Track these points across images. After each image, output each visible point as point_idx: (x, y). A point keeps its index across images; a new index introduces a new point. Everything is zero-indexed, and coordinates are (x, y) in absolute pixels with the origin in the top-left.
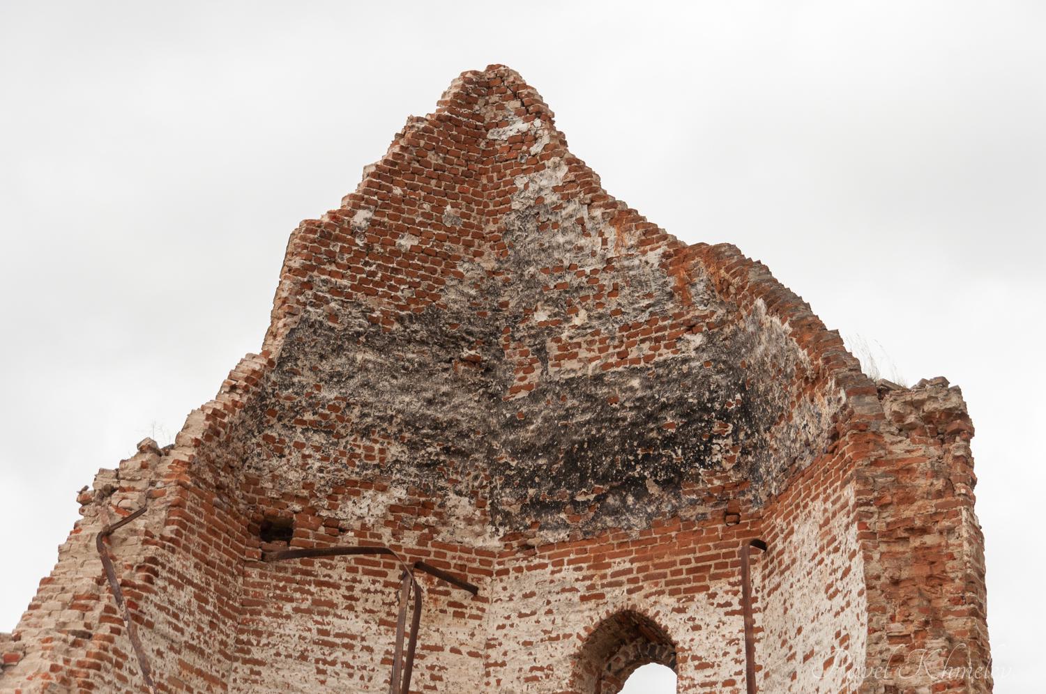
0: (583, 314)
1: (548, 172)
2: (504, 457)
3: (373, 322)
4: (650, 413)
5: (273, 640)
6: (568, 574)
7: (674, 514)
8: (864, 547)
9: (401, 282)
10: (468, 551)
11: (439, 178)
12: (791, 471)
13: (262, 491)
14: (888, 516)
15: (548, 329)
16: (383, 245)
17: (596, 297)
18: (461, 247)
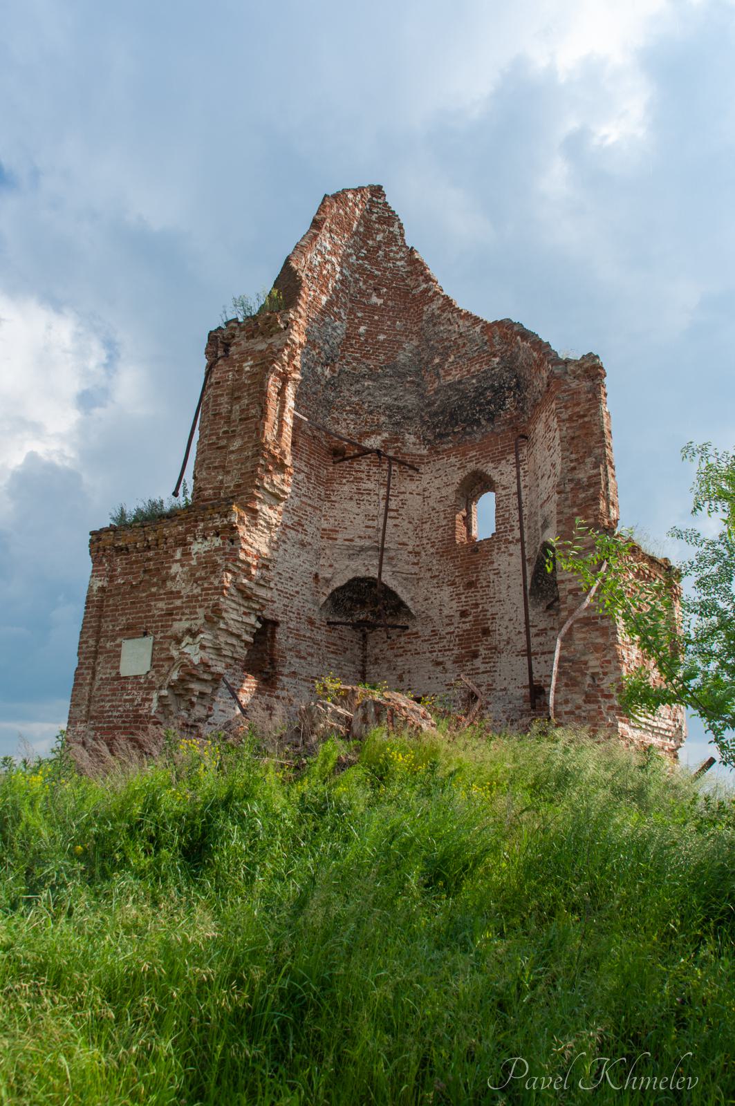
0: (452, 357)
1: (435, 302)
2: (427, 418)
3: (371, 370)
4: (480, 392)
5: (339, 493)
6: (453, 459)
7: (492, 431)
8: (559, 426)
9: (380, 353)
10: (415, 455)
11: (393, 311)
12: (536, 405)
14: (569, 412)
15: (440, 365)
16: (372, 339)
17: (457, 349)
18: (404, 338)
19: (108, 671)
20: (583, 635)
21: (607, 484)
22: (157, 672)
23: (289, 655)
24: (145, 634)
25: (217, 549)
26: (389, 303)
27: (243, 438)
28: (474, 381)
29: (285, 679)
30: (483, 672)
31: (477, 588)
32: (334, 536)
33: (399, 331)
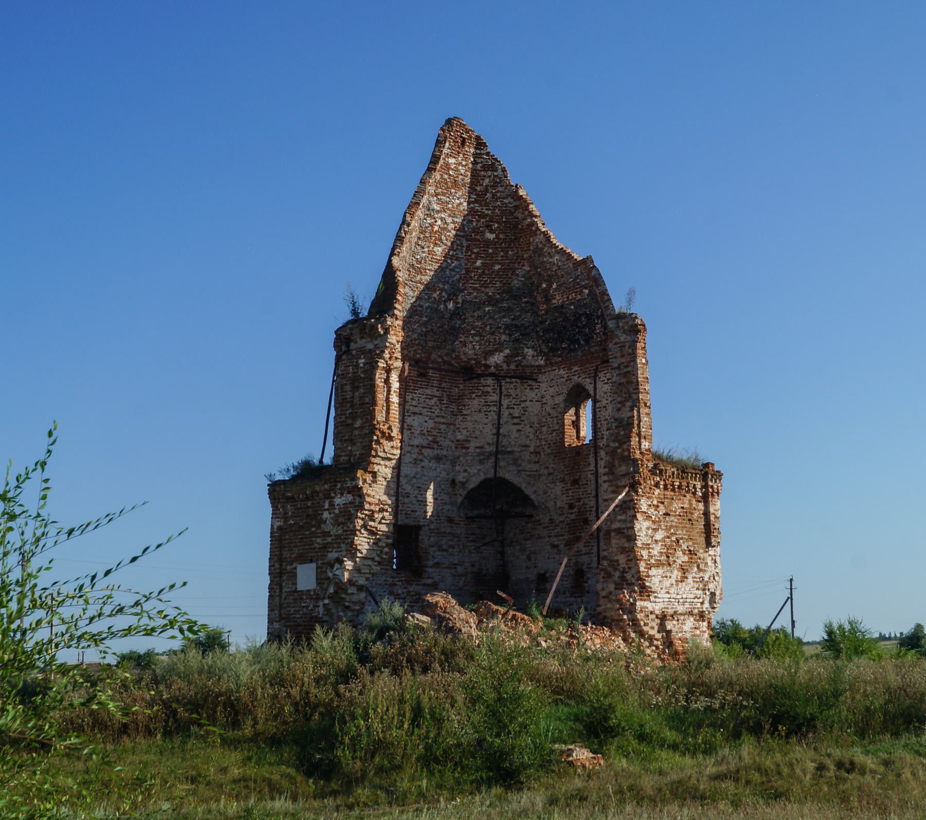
3: (490, 297)
6: (562, 372)
10: (532, 366)
13: (461, 359)
19: (290, 586)
20: (616, 541)
21: (640, 421)
22: (321, 587)
23: (431, 550)
24: (311, 561)
25: (351, 503)
26: (501, 236)
27: (362, 419)
28: (572, 307)
29: (430, 570)
30: (585, 554)
31: (579, 485)
32: (467, 445)
33: (512, 259)
